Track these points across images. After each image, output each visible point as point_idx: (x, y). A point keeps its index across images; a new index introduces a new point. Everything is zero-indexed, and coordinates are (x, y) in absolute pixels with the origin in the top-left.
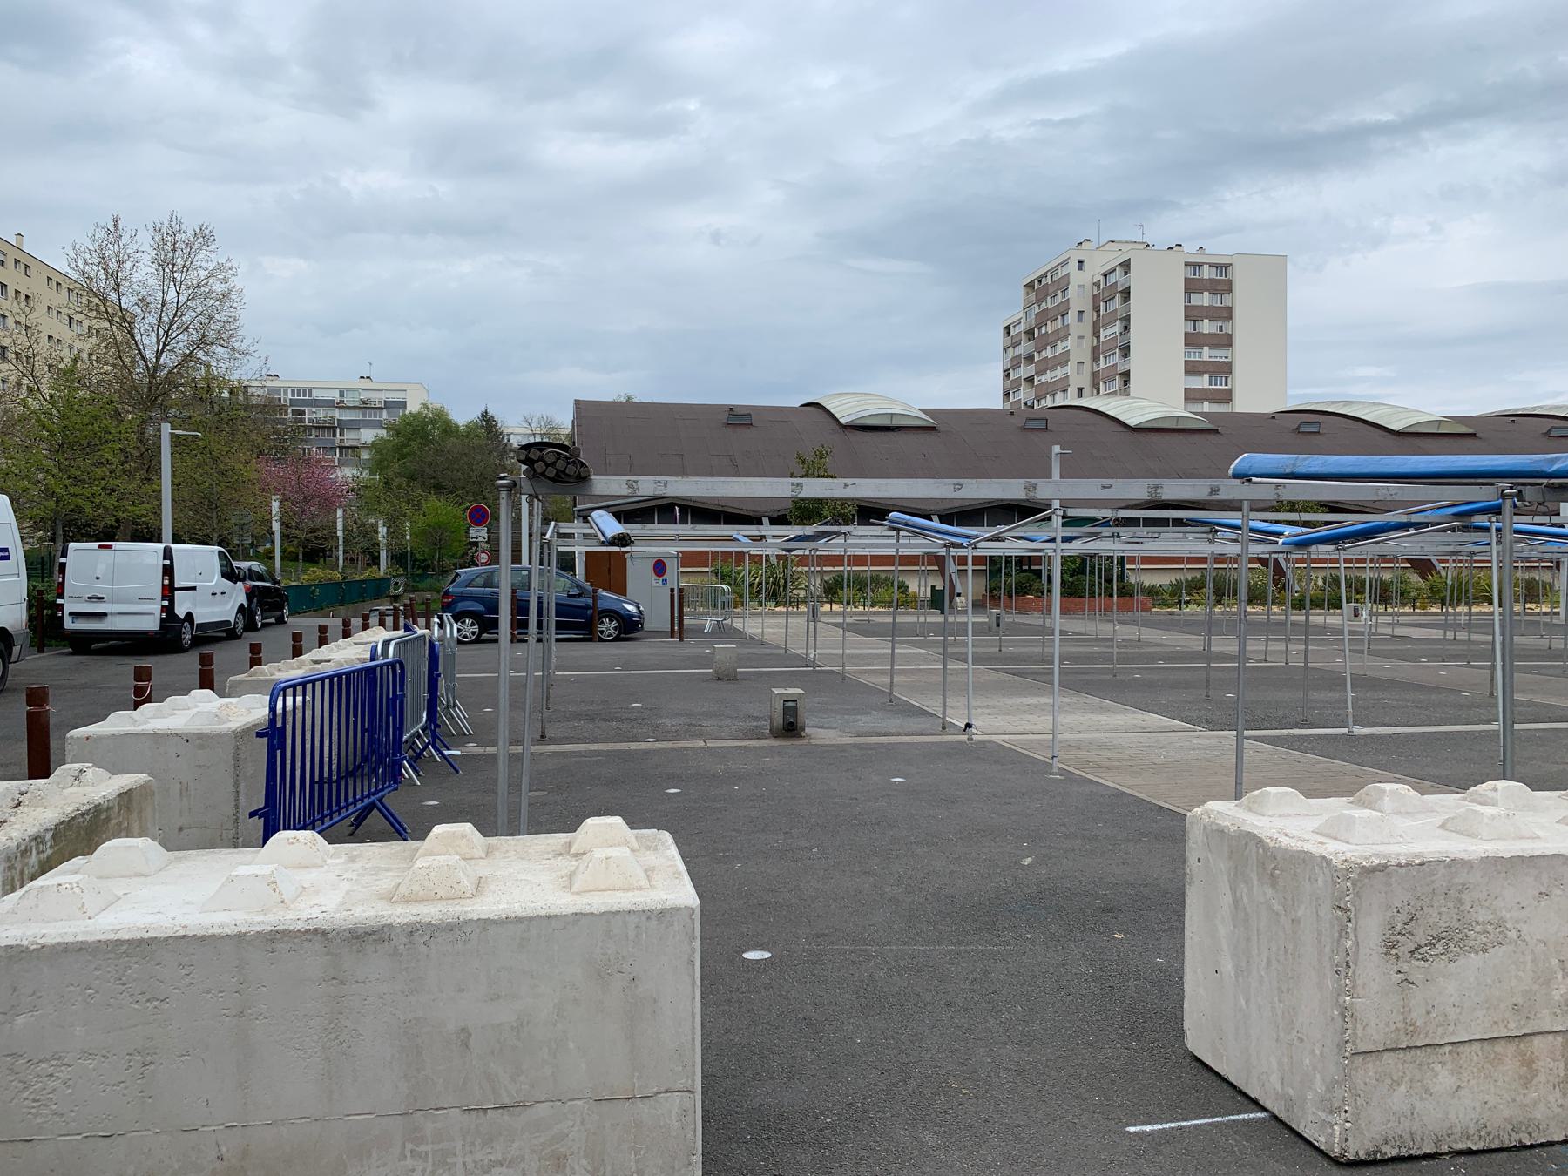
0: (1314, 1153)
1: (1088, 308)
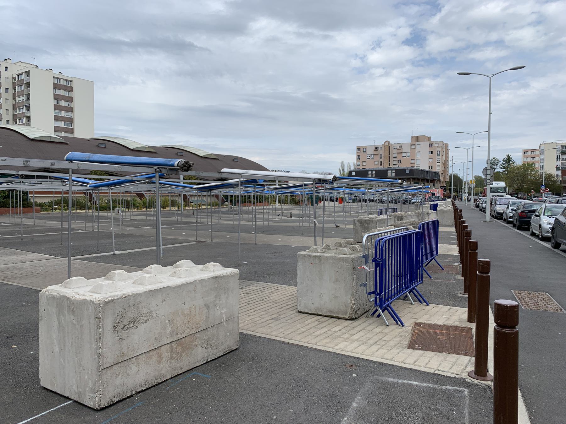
0: (89, 410)
1: (10, 87)
